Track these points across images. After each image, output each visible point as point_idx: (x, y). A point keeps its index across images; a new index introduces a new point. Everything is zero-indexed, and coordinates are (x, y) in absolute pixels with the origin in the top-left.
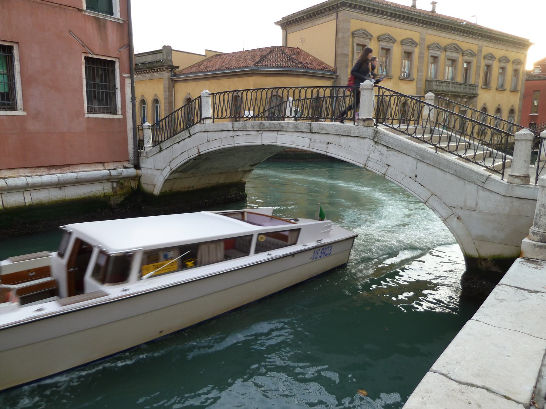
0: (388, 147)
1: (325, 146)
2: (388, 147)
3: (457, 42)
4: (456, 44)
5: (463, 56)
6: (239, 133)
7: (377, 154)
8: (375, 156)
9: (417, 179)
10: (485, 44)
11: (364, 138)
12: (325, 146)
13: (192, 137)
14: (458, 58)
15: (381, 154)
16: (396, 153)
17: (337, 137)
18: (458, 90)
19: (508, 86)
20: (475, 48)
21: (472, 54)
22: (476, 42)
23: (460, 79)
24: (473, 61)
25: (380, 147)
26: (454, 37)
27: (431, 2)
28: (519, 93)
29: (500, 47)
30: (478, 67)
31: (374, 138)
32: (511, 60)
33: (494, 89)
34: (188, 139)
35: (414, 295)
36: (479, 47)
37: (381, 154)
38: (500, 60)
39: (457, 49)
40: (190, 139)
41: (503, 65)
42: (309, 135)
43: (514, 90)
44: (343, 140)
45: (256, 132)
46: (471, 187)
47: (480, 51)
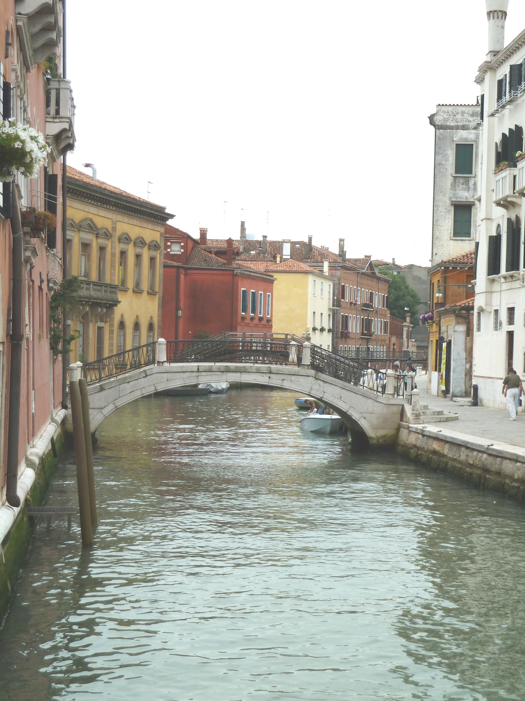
0: (324, 381)
1: (281, 382)
2: (324, 381)
3: (90, 216)
4: (91, 220)
5: (97, 237)
6: (203, 374)
7: (317, 385)
8: (316, 387)
9: (342, 399)
10: (119, 217)
11: (309, 376)
12: (281, 382)
13: (148, 377)
14: (92, 240)
15: (320, 385)
16: (329, 385)
17: (289, 376)
18: (98, 294)
19: (145, 286)
20: (108, 225)
21: (107, 235)
22: (110, 215)
23: (94, 277)
24: (107, 245)
25: (319, 382)
26: (93, 210)
27: (203, 226)
28: (157, 295)
29: (135, 222)
30: (113, 255)
31: (315, 376)
32: (147, 242)
33: (130, 291)
34: (143, 380)
35: (44, 656)
36: (113, 223)
37: (320, 385)
38: (135, 244)
39: (92, 227)
40: (145, 379)
41: (138, 250)
42: (268, 375)
43: (152, 293)
44: (293, 378)
45: (220, 373)
46: (370, 401)
47: (114, 229)
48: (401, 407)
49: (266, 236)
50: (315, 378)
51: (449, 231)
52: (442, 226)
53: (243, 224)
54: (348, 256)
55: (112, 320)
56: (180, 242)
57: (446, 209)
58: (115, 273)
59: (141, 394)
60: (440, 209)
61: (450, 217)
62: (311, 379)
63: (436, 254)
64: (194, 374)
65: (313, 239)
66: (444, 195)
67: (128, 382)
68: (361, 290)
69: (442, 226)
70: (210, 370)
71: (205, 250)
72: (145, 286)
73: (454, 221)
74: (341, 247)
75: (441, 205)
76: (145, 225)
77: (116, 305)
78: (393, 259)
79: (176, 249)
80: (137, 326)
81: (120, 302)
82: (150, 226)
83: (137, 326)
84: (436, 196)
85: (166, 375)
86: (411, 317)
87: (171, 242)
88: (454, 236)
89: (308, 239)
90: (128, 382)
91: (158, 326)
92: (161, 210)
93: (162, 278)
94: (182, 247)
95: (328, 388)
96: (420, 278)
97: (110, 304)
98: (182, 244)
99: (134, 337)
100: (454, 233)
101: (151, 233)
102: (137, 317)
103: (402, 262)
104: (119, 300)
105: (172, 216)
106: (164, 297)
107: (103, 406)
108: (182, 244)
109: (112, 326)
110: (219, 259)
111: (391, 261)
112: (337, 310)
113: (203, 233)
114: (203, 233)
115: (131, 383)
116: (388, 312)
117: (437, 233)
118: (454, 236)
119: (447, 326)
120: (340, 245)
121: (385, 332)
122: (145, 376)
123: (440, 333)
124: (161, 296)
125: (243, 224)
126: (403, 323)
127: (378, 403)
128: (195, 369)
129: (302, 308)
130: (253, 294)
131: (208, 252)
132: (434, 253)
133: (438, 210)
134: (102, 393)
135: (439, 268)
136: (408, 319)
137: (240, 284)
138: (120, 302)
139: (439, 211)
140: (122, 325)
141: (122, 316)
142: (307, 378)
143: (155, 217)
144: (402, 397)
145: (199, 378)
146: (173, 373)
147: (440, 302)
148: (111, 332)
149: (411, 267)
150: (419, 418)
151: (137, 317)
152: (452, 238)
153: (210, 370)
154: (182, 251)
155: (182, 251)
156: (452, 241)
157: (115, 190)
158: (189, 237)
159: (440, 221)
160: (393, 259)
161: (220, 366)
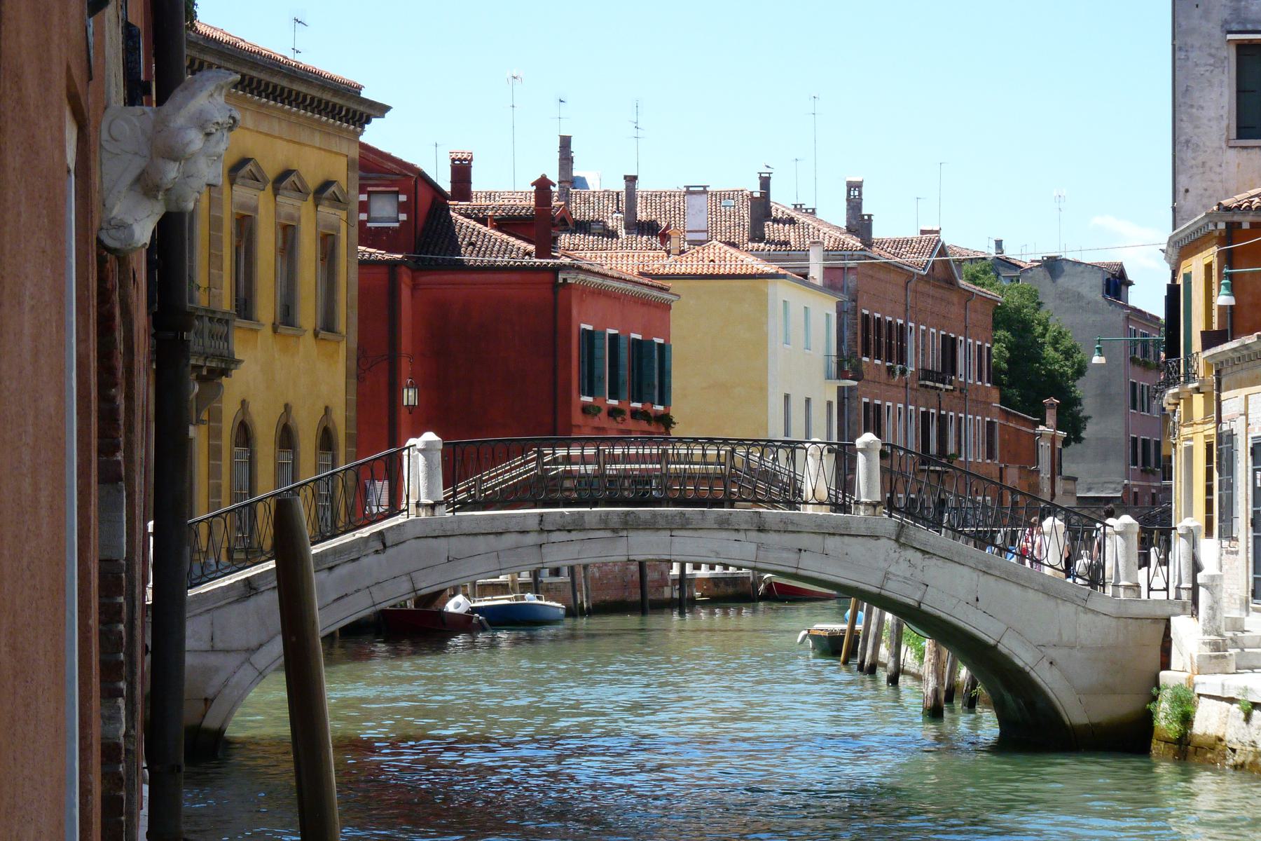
0: (924, 552)
9: (980, 604)
11: (877, 538)
13: (390, 551)
16: (940, 562)
19: (308, 313)
25: (910, 554)
27: (462, 147)
29: (276, 127)
40: (382, 557)
44: (832, 543)
45: (608, 534)
48: (1163, 627)
49: (635, 178)
50: (897, 540)
51: (1224, 123)
52: (1202, 108)
53: (565, 143)
54: (877, 233)
55: (216, 416)
56: (397, 193)
57: (1211, 55)
58: (221, 277)
59: (369, 602)
60: (1194, 55)
61: (1225, 78)
62: (887, 545)
63: (1187, 191)
64: (532, 539)
65: (772, 181)
66: (1206, 15)
67: (331, 569)
68: (917, 328)
69: (1202, 108)
70: (576, 526)
71: (468, 216)
72: (308, 313)
73: (1239, 91)
74: (854, 205)
75: (1197, 44)
76: (304, 135)
77: (225, 372)
78: (999, 244)
79: (386, 212)
80: (287, 438)
81: (240, 362)
82: (317, 139)
83: (287, 438)
84: (1180, 19)
85: (442, 541)
86: (1060, 414)
87: (370, 193)
88: (1239, 137)
89: (758, 182)
90: (331, 569)
91: (348, 436)
92: (352, 91)
93: (355, 292)
94: (402, 207)
95: (935, 571)
96: (1080, 297)
97: (211, 370)
98: (403, 198)
99: (279, 467)
100: (1238, 128)
101: (319, 157)
102: (287, 407)
103: (1026, 248)
104: (237, 357)
105: (382, 110)
106: (361, 347)
107: (254, 643)
108: (403, 198)
109: (215, 434)
110: (512, 239)
111: (992, 252)
112: (851, 388)
113: (461, 171)
114: (461, 171)
115: (337, 572)
116: (995, 394)
117: (1187, 127)
118: (1239, 137)
119: (1246, 397)
120: (848, 200)
121: (990, 455)
122: (380, 547)
123: (1219, 420)
124: (354, 345)
125: (565, 143)
126: (1036, 425)
127: (1090, 615)
128: (533, 524)
129: (773, 369)
130: (614, 338)
131: (478, 220)
132: (1181, 189)
133: (1187, 58)
134: (252, 602)
135: (1211, 227)
136: (1051, 417)
137: (575, 312)
138: (240, 362)
139: (1190, 63)
140: (244, 434)
141: (244, 403)
142: (872, 542)
143: (333, 111)
144: (1163, 595)
145: (544, 550)
146: (463, 538)
147: (1215, 327)
148: (215, 452)
149: (1053, 265)
150: (1224, 657)
151: (287, 407)
152: (1232, 143)
153: (576, 526)
154: (403, 217)
155: (403, 217)
156: (1232, 152)
157: (217, 35)
158: (422, 177)
159: (1197, 94)
160: (999, 244)
161: (608, 513)
